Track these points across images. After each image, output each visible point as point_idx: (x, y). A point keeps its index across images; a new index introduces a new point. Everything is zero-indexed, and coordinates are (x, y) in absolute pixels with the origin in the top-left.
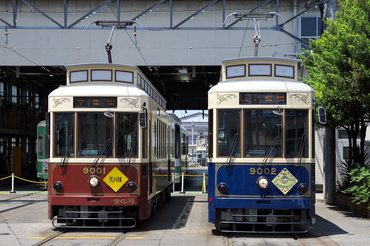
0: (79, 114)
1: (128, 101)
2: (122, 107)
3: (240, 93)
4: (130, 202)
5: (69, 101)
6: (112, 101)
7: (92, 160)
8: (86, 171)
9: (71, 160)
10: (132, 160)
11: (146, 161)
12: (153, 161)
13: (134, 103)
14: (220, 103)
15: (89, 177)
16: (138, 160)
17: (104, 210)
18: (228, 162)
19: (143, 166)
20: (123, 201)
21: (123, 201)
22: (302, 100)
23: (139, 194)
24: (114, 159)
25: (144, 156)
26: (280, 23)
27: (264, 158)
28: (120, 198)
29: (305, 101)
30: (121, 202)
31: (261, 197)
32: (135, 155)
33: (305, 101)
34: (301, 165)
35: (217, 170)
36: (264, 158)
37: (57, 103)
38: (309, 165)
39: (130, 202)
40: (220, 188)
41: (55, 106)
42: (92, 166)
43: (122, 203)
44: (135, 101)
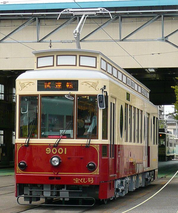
0: (43, 96)
1: (88, 84)
2: (83, 90)
3: (38, 81)
4: (89, 182)
5: (34, 84)
6: (74, 84)
7: (53, 141)
8: (48, 151)
9: (33, 141)
10: (93, 141)
11: (107, 142)
12: (116, 143)
13: (94, 86)
14: (22, 90)
15: (50, 156)
16: (100, 141)
17: (65, 189)
18: (26, 142)
19: (104, 147)
20: (82, 181)
21: (82, 181)
22: (92, 86)
23: (98, 174)
24: (75, 139)
25: (105, 137)
26: (165, 36)
27: (26, 139)
28: (80, 178)
29: (95, 88)
30: (81, 181)
31: (54, 174)
32: (96, 137)
33: (95, 88)
34: (90, 145)
35: (18, 150)
36: (26, 139)
37: (23, 86)
38: (99, 146)
39: (89, 182)
40: (20, 166)
41: (20, 90)
42: (54, 146)
43: (82, 182)
44: (95, 84)
